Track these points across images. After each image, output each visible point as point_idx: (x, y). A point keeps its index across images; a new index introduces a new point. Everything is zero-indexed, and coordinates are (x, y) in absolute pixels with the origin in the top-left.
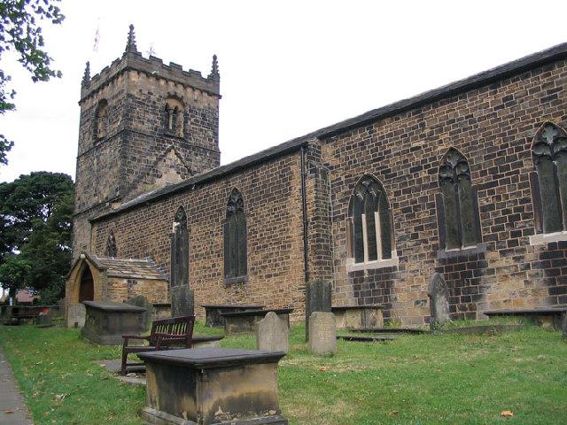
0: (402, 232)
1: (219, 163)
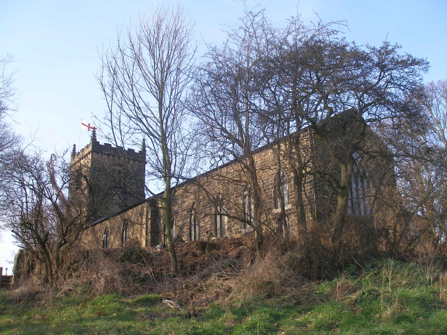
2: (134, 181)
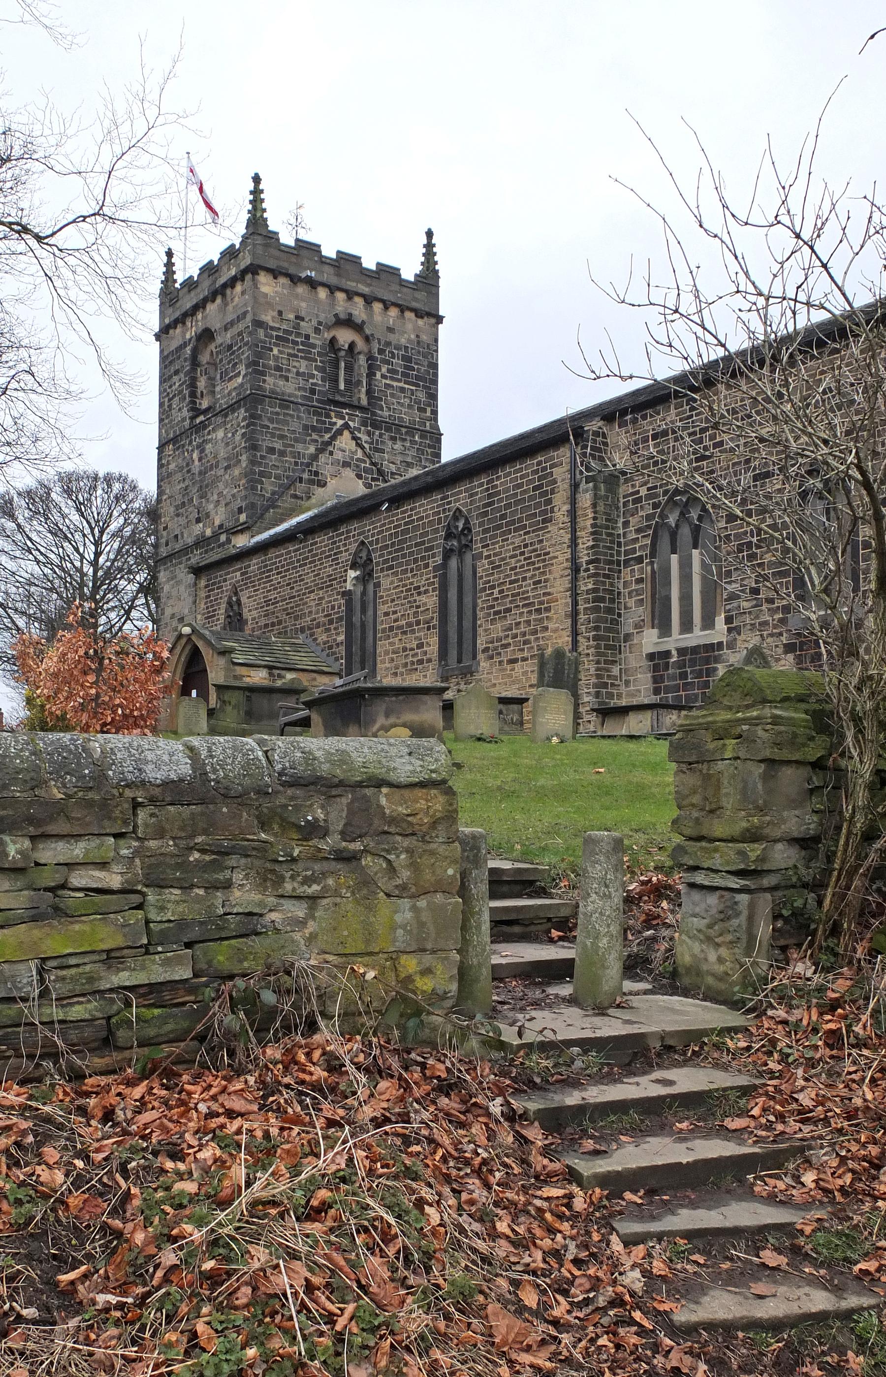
0: (734, 585)
1: (438, 455)
2: (401, 384)
